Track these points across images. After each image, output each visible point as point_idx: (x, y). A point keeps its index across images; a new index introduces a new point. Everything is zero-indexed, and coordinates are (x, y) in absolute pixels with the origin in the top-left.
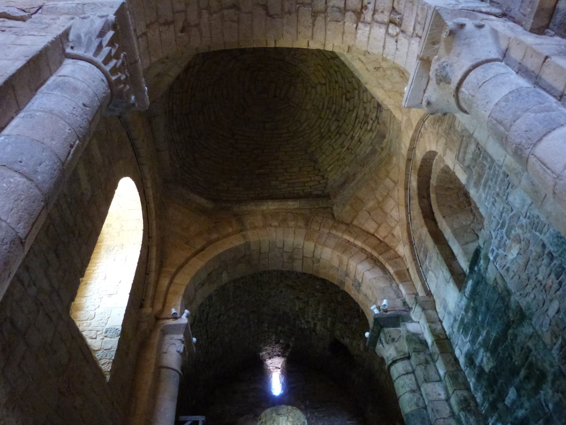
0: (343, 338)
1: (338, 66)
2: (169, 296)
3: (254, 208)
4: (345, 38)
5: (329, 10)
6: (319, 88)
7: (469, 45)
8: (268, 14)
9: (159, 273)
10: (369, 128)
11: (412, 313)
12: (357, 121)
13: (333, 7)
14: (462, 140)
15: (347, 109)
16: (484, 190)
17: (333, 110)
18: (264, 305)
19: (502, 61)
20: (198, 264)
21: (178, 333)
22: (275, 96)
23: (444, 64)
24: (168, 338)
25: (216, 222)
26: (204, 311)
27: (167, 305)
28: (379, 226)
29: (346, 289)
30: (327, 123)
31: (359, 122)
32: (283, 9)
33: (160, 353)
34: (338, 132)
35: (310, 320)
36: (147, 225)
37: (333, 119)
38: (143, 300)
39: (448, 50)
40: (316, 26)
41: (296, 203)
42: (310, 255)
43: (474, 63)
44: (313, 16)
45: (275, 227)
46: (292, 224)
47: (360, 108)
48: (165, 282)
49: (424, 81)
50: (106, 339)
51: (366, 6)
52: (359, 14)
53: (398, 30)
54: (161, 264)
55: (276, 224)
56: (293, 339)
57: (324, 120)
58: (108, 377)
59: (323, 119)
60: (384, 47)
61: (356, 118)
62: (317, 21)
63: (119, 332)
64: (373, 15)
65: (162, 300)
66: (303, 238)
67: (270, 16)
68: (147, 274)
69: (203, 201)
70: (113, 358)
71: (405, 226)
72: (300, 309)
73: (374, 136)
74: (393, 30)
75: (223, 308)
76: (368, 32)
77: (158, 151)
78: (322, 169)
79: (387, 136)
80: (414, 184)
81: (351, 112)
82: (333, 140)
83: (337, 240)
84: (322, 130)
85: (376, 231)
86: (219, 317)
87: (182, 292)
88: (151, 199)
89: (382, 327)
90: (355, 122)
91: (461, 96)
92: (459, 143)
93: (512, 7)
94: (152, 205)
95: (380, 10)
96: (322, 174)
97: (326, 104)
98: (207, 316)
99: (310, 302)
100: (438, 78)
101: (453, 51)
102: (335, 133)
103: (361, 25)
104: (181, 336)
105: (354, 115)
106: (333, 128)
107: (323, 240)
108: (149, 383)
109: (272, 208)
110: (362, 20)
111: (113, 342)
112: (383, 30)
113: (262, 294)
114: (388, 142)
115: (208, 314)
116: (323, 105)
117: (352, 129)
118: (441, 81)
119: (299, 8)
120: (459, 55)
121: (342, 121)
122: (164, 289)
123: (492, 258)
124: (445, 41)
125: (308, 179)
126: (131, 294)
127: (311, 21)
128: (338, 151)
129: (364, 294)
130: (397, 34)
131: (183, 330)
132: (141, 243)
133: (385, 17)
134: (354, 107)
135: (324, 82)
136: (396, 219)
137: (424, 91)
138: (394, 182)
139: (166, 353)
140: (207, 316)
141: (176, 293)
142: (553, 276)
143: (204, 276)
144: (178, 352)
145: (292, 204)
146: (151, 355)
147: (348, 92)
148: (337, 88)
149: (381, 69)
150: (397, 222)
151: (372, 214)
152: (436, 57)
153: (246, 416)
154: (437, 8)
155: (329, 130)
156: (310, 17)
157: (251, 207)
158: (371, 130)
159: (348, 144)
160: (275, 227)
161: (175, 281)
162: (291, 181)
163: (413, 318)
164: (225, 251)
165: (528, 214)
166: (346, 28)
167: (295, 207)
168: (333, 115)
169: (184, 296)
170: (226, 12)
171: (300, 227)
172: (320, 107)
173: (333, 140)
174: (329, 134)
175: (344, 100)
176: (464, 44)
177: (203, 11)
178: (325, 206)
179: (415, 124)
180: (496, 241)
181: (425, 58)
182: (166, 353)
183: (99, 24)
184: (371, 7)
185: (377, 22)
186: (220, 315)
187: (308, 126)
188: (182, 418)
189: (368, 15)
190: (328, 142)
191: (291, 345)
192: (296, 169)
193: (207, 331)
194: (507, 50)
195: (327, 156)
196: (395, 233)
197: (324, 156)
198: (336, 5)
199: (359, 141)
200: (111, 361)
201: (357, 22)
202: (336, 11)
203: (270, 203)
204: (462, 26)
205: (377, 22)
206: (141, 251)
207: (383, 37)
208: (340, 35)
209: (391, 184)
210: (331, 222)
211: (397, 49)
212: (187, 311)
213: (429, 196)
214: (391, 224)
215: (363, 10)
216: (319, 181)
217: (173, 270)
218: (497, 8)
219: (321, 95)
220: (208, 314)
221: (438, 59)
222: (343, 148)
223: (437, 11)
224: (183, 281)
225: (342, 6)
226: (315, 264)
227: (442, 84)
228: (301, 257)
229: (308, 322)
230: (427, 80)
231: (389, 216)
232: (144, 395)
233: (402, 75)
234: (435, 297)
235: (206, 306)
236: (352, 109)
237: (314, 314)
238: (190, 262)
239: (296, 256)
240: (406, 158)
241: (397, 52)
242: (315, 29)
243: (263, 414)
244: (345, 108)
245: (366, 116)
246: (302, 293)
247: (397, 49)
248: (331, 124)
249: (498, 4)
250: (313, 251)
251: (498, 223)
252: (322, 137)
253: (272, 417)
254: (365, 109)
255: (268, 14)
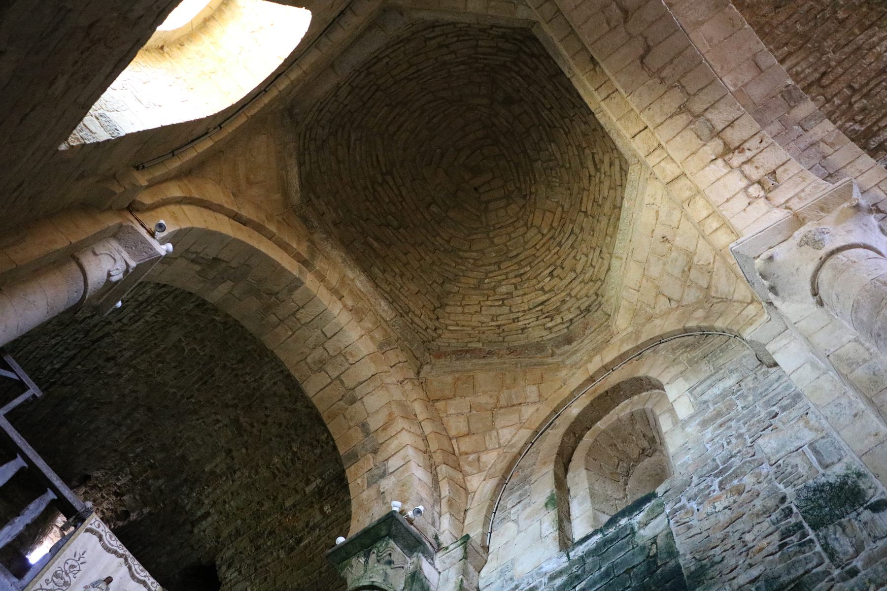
0: (229, 567)
1: (582, 229)
3: (340, 260)
4: (690, 159)
5: (702, 119)
6: (532, 233)
8: (642, 58)
9: (185, 174)
10: (550, 325)
11: (439, 554)
12: (539, 308)
13: (708, 120)
15: (540, 285)
16: (715, 429)
17: (522, 271)
18: (173, 416)
21: (133, 256)
22: (475, 189)
24: (114, 245)
26: (110, 323)
28: (469, 434)
29: (350, 473)
30: (500, 278)
31: (541, 310)
32: (660, 70)
33: (89, 244)
34: (503, 300)
35: (206, 502)
37: (514, 281)
38: (144, 167)
39: (838, 222)
40: (672, 120)
42: (349, 383)
44: (680, 107)
45: (345, 306)
47: (558, 297)
48: (175, 191)
49: (780, 238)
51: (743, 150)
52: (728, 150)
53: (762, 193)
56: (146, 511)
57: (500, 272)
58: (63, 147)
59: (500, 269)
60: (728, 200)
61: (542, 303)
62: (678, 117)
64: (744, 163)
67: (642, 62)
69: (295, 182)
70: (88, 142)
71: (509, 457)
72: (212, 473)
73: (548, 337)
74: (755, 190)
75: (128, 354)
76: (722, 174)
77: (332, 66)
78: (442, 321)
79: (574, 344)
80: (575, 410)
81: (540, 292)
82: (489, 303)
84: (486, 281)
85: (458, 438)
86: (108, 360)
87: (184, 226)
88: (274, 93)
89: (390, 535)
90: (535, 307)
94: (266, 99)
95: (756, 164)
96: (437, 325)
97: (521, 257)
98: (102, 337)
99: (238, 474)
102: (497, 297)
103: (720, 162)
104: (133, 264)
105: (544, 298)
106: (503, 289)
110: (726, 158)
111: (103, 136)
112: (744, 183)
113: (192, 396)
114: (567, 351)
115: (108, 335)
116: (517, 255)
117: (524, 311)
119: (676, 86)
121: (521, 292)
123: (667, 511)
124: (842, 212)
125: (418, 313)
127: (673, 110)
128: (483, 319)
129: (378, 491)
130: (757, 198)
131: (145, 258)
133: (756, 175)
134: (550, 291)
135: (545, 231)
136: (501, 442)
138: (540, 396)
139: (95, 254)
140: (102, 337)
142: (776, 537)
143: (212, 252)
144: (109, 275)
146: (87, 228)
147: (563, 268)
148: (554, 252)
149: (669, 245)
150: (500, 447)
151: (474, 412)
155: (494, 289)
156: (677, 106)
158: (550, 328)
159: (503, 322)
163: (437, 562)
164: (267, 256)
165: (780, 462)
166: (701, 151)
167: (384, 315)
168: (516, 277)
169: (180, 230)
171: (372, 338)
172: (511, 255)
173: (489, 303)
174: (491, 292)
175: (548, 271)
179: (644, 338)
180: (696, 490)
181: (801, 216)
182: (95, 254)
184: (749, 154)
185: (742, 172)
186: (114, 358)
187: (475, 260)
189: (737, 159)
190: (481, 299)
191: (133, 516)
192: (414, 288)
193: (72, 358)
195: (463, 313)
196: (484, 458)
197: (460, 309)
198: (713, 122)
199: (523, 329)
200: (83, 141)
201: (722, 156)
202: (708, 127)
203: (363, 278)
205: (742, 172)
206: (208, 117)
207: (737, 190)
208: (687, 153)
209: (534, 397)
211: (745, 210)
212: (170, 247)
213: (580, 438)
214: (487, 443)
215: (737, 151)
216: (427, 328)
217: (196, 195)
219: (526, 243)
220: (108, 335)
222: (492, 320)
224: (194, 219)
225: (720, 127)
226: (341, 403)
228: (335, 374)
229: (200, 503)
231: (494, 433)
233: (686, 269)
234: (490, 557)
235: (120, 320)
236: (546, 289)
237: (224, 497)
239: (329, 368)
240: (604, 363)
241: (742, 213)
242: (668, 121)
244: (539, 282)
245: (558, 310)
246: (244, 451)
247: (745, 210)
248: (503, 283)
250: (361, 380)
251: (717, 467)
252: (478, 287)
254: (563, 302)
255: (642, 58)
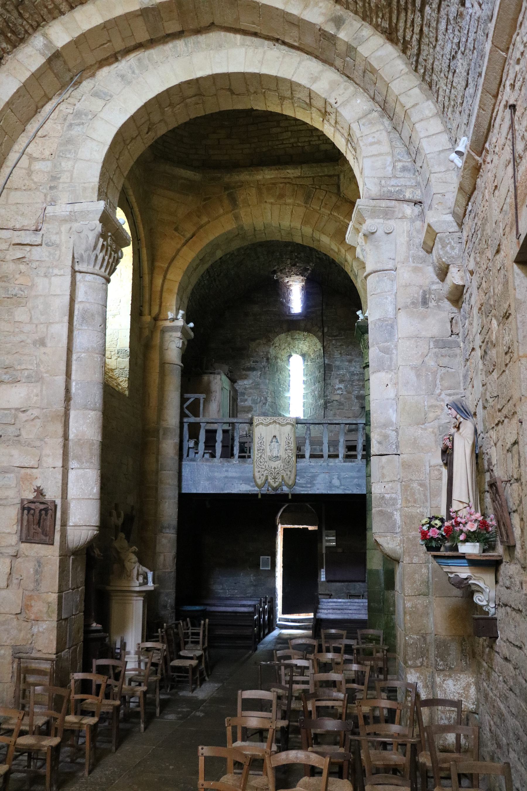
2: (164, 294)
20: (189, 255)
25: (205, 200)
27: (163, 304)
33: (162, 350)
36: (137, 260)
41: (296, 171)
46: (289, 201)
48: (158, 281)
50: (119, 359)
54: (153, 260)
55: (272, 200)
63: (128, 353)
65: (158, 301)
66: (301, 221)
68: (141, 277)
83: (338, 223)
107: (322, 224)
108: (157, 381)
109: (268, 177)
122: (159, 289)
126: (131, 315)
132: (132, 254)
141: (170, 291)
145: (292, 172)
146: (155, 356)
153: (258, 341)
157: (244, 176)
160: (272, 203)
161: (168, 276)
162: (296, 128)
170: (188, 101)
171: (299, 205)
177: (166, 109)
178: (331, 173)
183: (92, 239)
188: (186, 396)
210: (334, 199)
224: (176, 276)
232: (154, 392)
238: (181, 253)
243: (277, 338)
253: (287, 341)
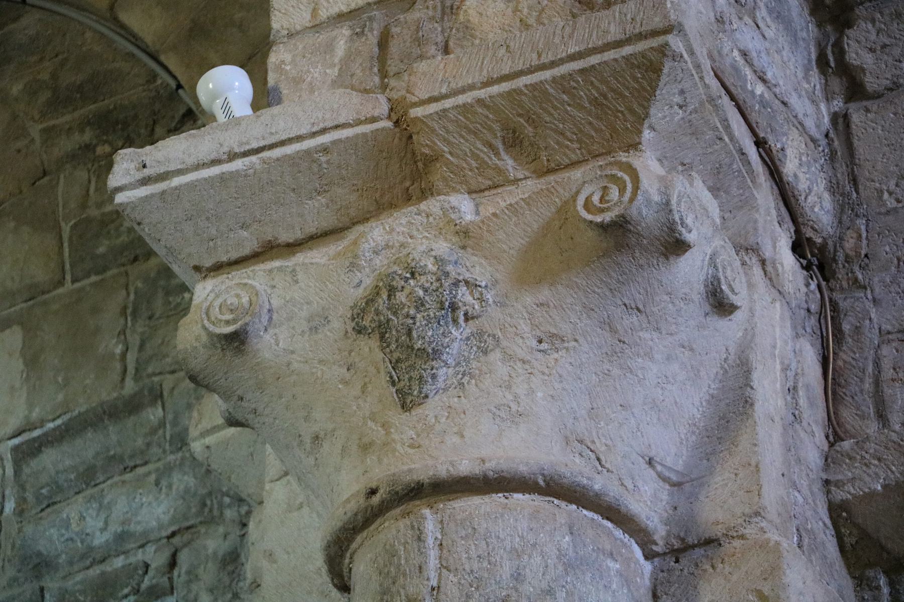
7: (620, 346)
14: (133, 406)
19: (649, 556)
23: (464, 295)
43: (575, 467)
49: (315, 214)
91: (392, 529)
92: (106, 394)
93: (878, 280)
100: (382, 301)
101: (545, 294)
118: (382, 331)
120: (550, 341)
137: (269, 250)
152: (465, 207)
154: (675, 42)
176: (609, 325)
181: (423, 143)
194: (710, 542)
204: (676, 246)
218: (834, 188)
221: (465, 236)
223: (663, 50)
227: (369, 346)
230: (327, 221)
249: (854, 181)
